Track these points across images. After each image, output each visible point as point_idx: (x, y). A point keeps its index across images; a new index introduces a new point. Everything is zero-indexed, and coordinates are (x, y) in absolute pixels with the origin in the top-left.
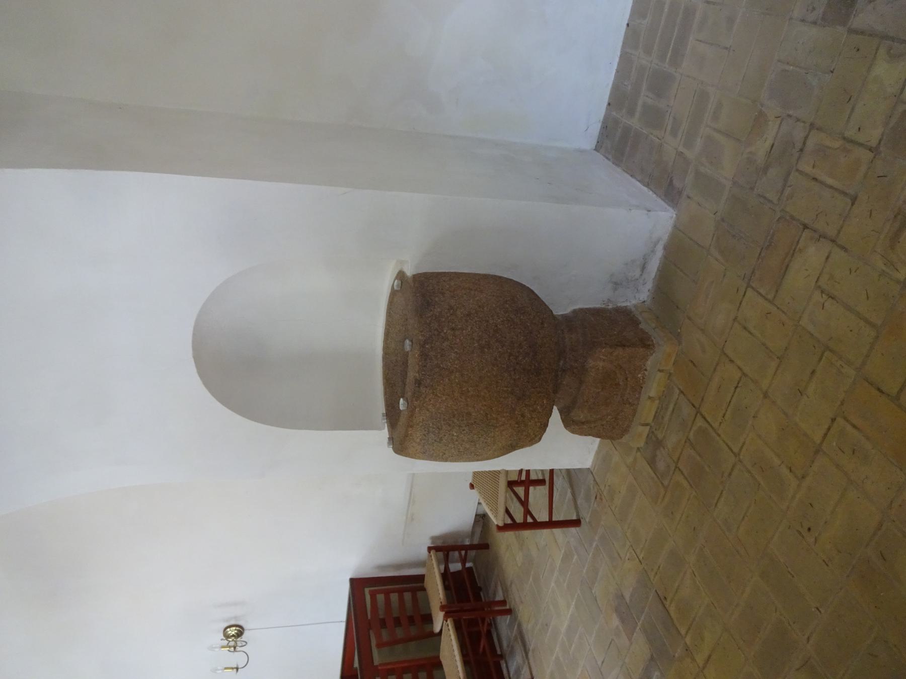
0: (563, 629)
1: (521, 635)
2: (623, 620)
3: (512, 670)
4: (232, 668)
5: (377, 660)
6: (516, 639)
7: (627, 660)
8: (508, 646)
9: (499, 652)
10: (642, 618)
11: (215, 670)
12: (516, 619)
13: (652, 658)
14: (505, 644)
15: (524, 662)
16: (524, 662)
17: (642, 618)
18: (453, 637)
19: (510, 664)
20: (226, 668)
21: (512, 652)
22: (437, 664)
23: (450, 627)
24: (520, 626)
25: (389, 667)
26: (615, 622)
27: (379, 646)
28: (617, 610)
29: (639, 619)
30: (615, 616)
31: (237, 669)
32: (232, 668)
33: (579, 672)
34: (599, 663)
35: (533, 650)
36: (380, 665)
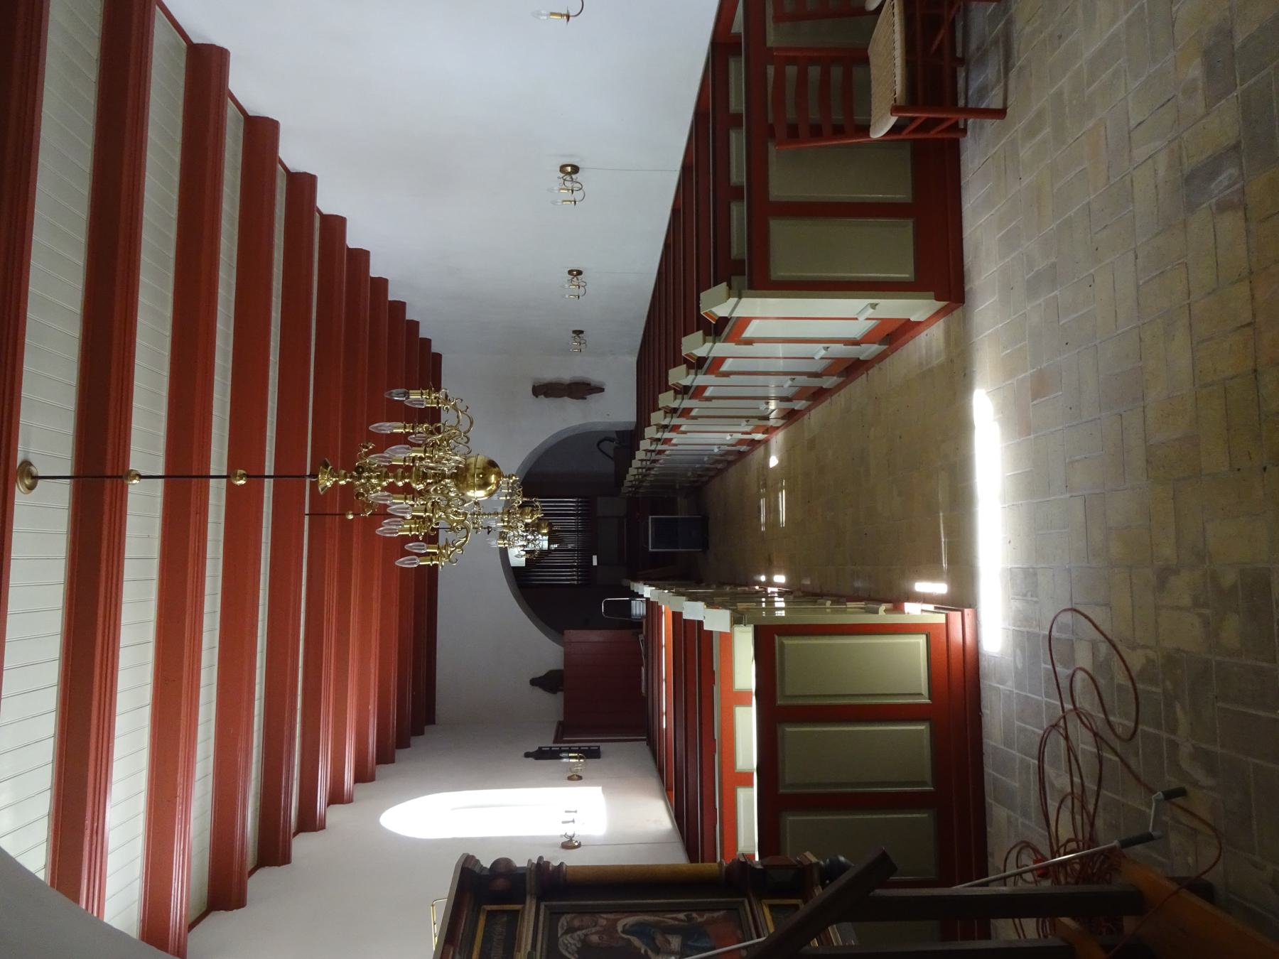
0: (1088, 53)
1: (1006, 42)
2: (1210, 70)
3: (974, 85)
4: (562, 15)
5: (771, 41)
6: (996, 42)
7: (1185, 135)
8: (978, 49)
9: (959, 54)
10: (1252, 81)
11: (537, 14)
12: (1006, 10)
13: (1236, 147)
14: (973, 45)
15: (998, 81)
16: (998, 81)
17: (1252, 81)
18: (897, 21)
19: (973, 75)
20: (552, 14)
21: (982, 61)
22: (861, 58)
23: (896, 11)
24: (1009, 23)
25: (791, 54)
26: (1195, 71)
27: (778, 18)
28: (1208, 56)
29: (1243, 81)
30: (1198, 61)
31: (568, 17)
32: (562, 15)
33: (1091, 124)
34: (1133, 123)
35: (1021, 68)
36: (778, 49)
